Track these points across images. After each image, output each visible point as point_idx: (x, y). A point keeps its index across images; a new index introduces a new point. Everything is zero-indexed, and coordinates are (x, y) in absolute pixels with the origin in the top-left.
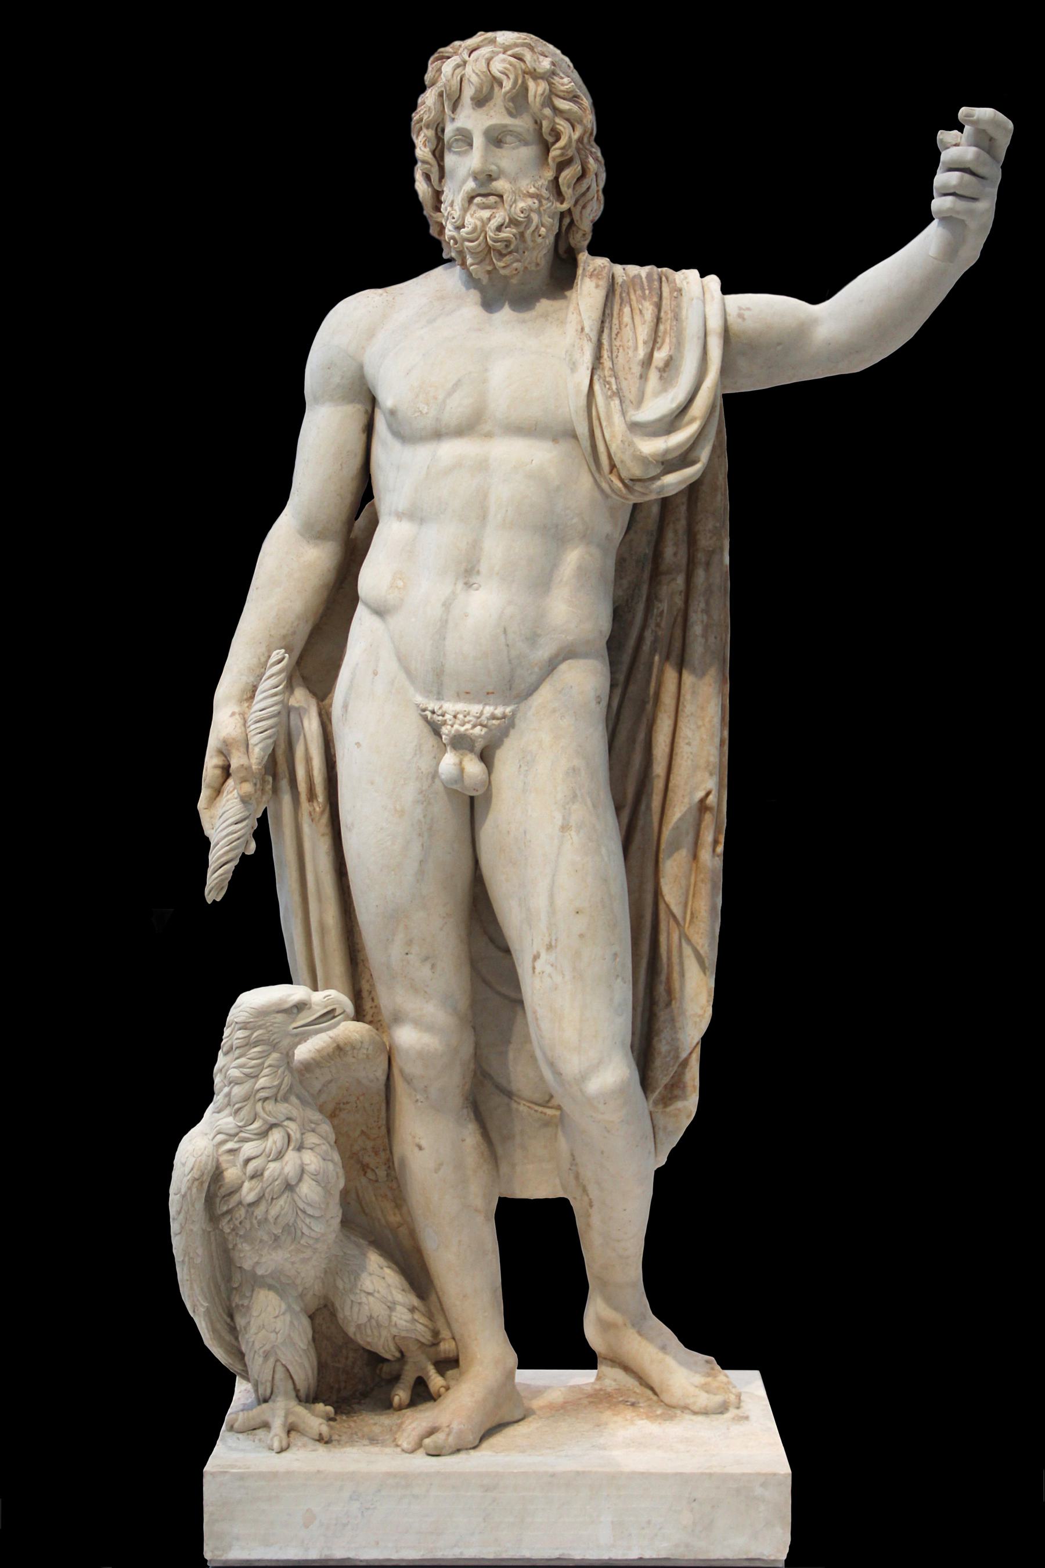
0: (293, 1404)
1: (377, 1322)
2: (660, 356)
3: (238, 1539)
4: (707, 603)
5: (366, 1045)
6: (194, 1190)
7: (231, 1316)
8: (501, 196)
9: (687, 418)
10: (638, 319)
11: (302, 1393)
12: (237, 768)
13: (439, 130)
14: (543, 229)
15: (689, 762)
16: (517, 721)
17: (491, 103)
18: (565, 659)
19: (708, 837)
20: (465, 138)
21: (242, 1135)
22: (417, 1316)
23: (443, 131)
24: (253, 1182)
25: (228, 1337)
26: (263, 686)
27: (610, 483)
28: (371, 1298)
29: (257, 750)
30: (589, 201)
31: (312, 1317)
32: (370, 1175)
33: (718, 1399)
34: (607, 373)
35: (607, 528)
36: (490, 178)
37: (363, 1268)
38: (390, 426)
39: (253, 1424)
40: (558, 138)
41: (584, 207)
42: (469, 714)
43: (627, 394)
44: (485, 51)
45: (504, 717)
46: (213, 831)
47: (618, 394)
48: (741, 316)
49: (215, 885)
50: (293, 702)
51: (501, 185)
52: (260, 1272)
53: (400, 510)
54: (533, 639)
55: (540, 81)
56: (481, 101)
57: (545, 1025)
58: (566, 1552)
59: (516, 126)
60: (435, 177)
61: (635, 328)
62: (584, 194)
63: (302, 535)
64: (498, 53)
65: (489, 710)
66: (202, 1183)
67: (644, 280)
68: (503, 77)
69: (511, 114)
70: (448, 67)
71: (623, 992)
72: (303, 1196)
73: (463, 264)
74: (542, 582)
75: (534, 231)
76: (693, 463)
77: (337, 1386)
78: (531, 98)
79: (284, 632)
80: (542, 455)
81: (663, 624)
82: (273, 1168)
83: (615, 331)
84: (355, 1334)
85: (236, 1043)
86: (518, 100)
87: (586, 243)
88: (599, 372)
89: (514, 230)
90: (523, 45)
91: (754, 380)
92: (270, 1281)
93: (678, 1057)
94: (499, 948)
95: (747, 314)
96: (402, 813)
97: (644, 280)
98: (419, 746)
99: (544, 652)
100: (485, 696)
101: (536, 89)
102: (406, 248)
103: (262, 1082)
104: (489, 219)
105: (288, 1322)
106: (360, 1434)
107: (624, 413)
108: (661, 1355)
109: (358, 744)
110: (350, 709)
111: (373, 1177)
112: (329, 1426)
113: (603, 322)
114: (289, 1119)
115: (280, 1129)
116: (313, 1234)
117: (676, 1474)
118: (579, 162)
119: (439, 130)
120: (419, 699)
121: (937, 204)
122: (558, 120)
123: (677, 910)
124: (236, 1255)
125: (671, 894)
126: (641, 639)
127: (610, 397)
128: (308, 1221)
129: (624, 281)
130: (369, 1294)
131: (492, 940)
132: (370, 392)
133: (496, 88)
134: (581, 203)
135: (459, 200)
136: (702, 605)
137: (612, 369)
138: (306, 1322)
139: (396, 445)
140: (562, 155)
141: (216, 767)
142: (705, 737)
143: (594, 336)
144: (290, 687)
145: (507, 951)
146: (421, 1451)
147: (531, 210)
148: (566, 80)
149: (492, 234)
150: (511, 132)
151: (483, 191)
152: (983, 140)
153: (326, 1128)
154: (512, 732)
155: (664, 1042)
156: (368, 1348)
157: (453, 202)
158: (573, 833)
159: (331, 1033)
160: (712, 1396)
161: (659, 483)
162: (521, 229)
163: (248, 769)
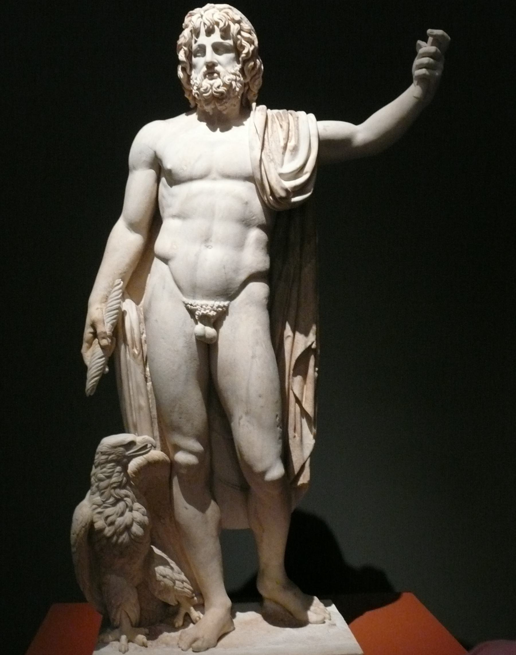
2: (291, 144)
11: (134, 623)
20: (202, 50)
23: (191, 47)
24: (110, 527)
31: (136, 587)
44: (212, 11)
45: (224, 306)
47: (272, 160)
48: (325, 129)
49: (91, 382)
70: (194, 18)
74: (240, 245)
79: (120, 272)
82: (119, 521)
86: (225, 33)
87: (256, 98)
99: (243, 277)
102: (173, 101)
103: (114, 479)
107: (276, 169)
121: (417, 72)
132: (159, 164)
141: (91, 333)
144: (123, 298)
146: (191, 649)
149: (215, 90)
152: (437, 41)
158: (257, 360)
159: (145, 456)
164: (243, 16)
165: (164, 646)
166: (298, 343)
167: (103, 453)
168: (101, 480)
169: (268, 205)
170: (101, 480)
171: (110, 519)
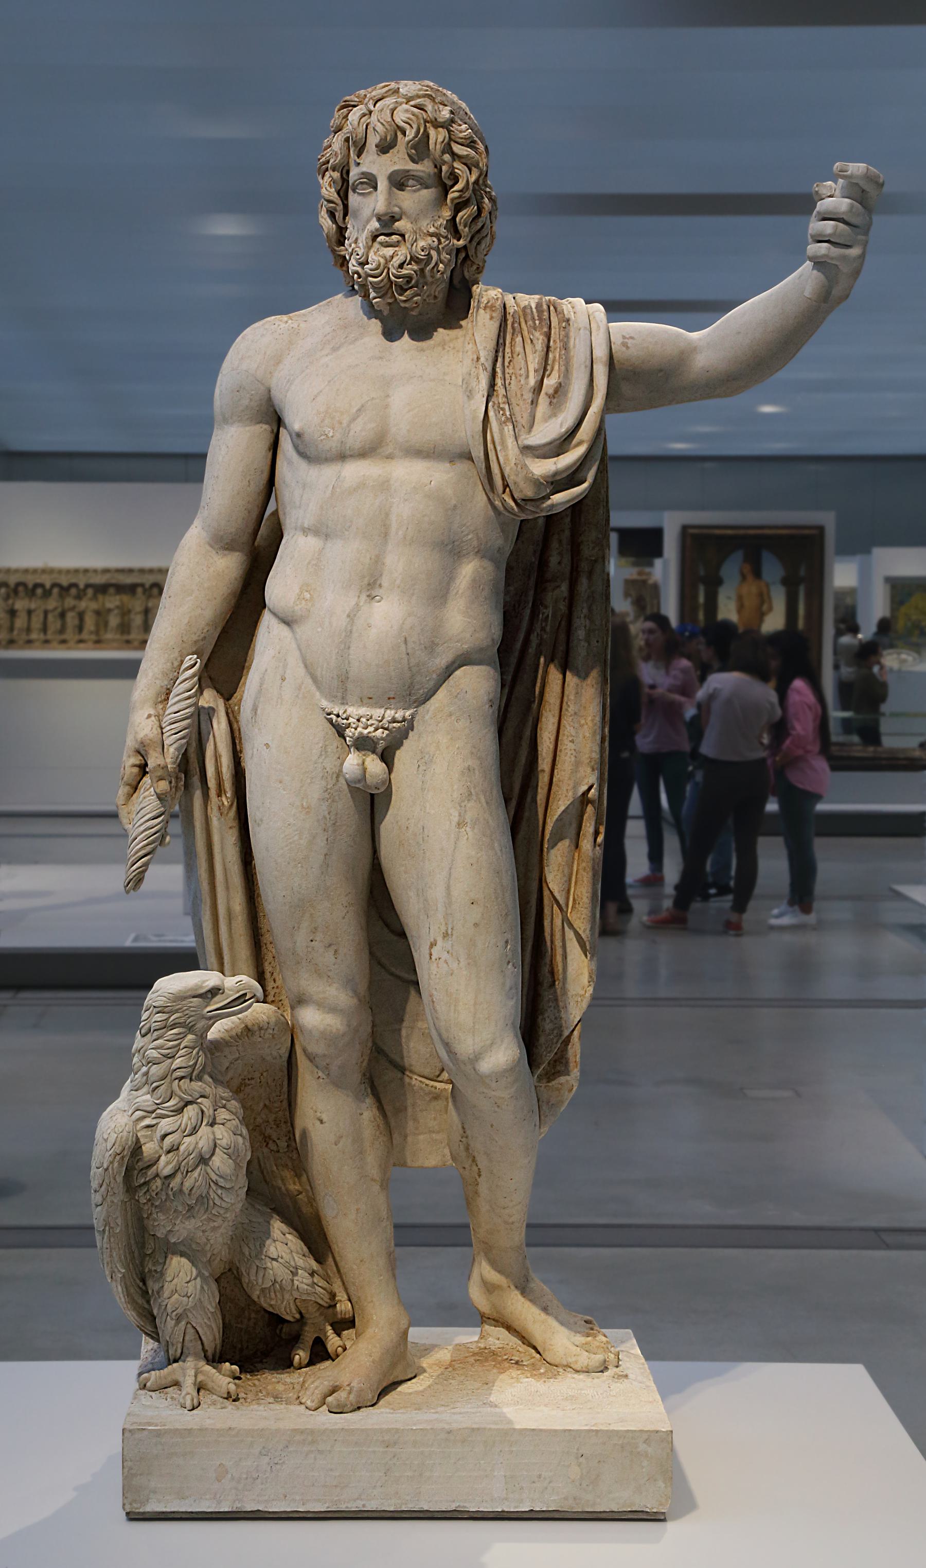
0: (202, 1363)
1: (281, 1287)
2: (550, 383)
3: (155, 1492)
4: (590, 610)
5: (272, 1024)
6: (116, 1164)
7: (144, 1281)
8: (403, 236)
11: (210, 1354)
12: (154, 768)
13: (344, 172)
14: (441, 265)
15: (573, 759)
17: (394, 150)
18: (460, 666)
19: (589, 827)
20: (371, 181)
22: (316, 1279)
23: (348, 172)
25: (140, 1301)
26: (178, 688)
27: (503, 501)
28: (274, 1263)
29: (172, 750)
30: (483, 238)
31: (217, 1280)
32: (272, 1146)
33: (599, 1357)
34: (501, 400)
35: (500, 542)
36: (394, 219)
37: (268, 1234)
38: (296, 447)
39: (164, 1382)
41: (479, 243)
42: (371, 718)
43: (519, 419)
44: (389, 101)
45: (404, 720)
46: (131, 826)
47: (512, 420)
48: (624, 344)
50: (202, 703)
53: (306, 525)
54: (431, 648)
55: (440, 129)
56: (385, 148)
57: (441, 1008)
58: (462, 1504)
59: (417, 171)
60: (339, 215)
62: (479, 231)
63: (211, 546)
64: (401, 104)
65: (389, 714)
66: (123, 1157)
67: (534, 310)
69: (414, 161)
71: (513, 975)
72: (215, 1169)
73: (366, 296)
74: (439, 595)
75: (433, 268)
77: (239, 1346)
78: (431, 146)
79: (195, 638)
81: (548, 629)
83: (507, 360)
84: (259, 1297)
86: (420, 149)
88: (494, 399)
89: (415, 267)
92: (182, 1248)
93: (561, 1035)
94: (393, 932)
95: (630, 342)
96: (307, 810)
97: (534, 310)
98: (325, 748)
99: (441, 661)
100: (388, 700)
103: (178, 1062)
105: (199, 1287)
106: (264, 1393)
108: (543, 1316)
109: (267, 745)
110: (259, 712)
111: (275, 1148)
112: (235, 1384)
113: (497, 351)
115: (195, 1105)
116: (224, 1205)
117: (565, 1431)
118: (475, 202)
119: (344, 172)
120: (325, 703)
122: (456, 165)
124: (149, 1223)
125: (554, 881)
126: (527, 641)
127: (505, 422)
128: (219, 1192)
129: (515, 311)
130: (273, 1259)
131: (387, 925)
134: (476, 240)
135: (364, 237)
136: (585, 611)
138: (214, 1286)
139: (302, 464)
140: (460, 197)
142: (588, 735)
143: (489, 366)
145: (402, 934)
147: (431, 248)
148: (464, 126)
149: (394, 271)
150: (414, 177)
155: (548, 1021)
156: (271, 1310)
157: (357, 239)
160: (593, 1356)
161: (549, 502)
162: (422, 266)
165: (271, 1400)
166: (558, 786)
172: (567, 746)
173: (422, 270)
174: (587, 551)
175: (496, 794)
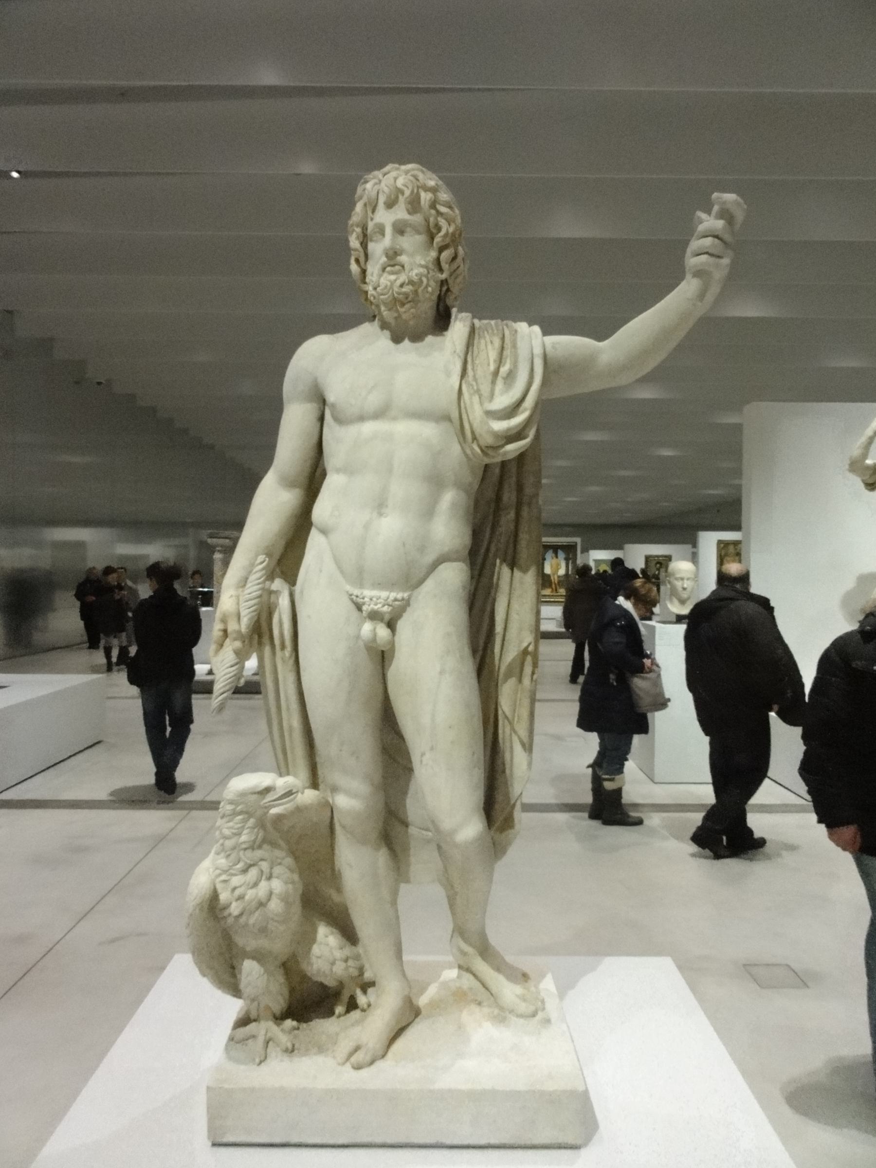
2: (504, 370)
8: (403, 267)
9: (521, 409)
10: (490, 347)
16: (411, 602)
21: (232, 871)
26: (253, 577)
27: (472, 449)
40: (439, 229)
41: (456, 278)
44: (394, 174)
45: (403, 599)
47: (478, 391)
48: (553, 347)
51: (403, 259)
52: (248, 949)
54: (422, 549)
56: (390, 205)
60: (362, 259)
61: (487, 351)
62: (455, 271)
65: (393, 595)
68: (405, 189)
69: (410, 213)
70: (369, 186)
71: (479, 775)
74: (429, 512)
76: (524, 438)
78: (422, 202)
80: (429, 431)
82: (250, 894)
85: (228, 812)
86: (414, 205)
90: (418, 170)
91: (561, 391)
99: (430, 558)
101: (425, 197)
103: (244, 838)
104: (396, 280)
107: (481, 404)
114: (262, 860)
120: (348, 588)
121: (692, 262)
122: (439, 219)
123: (508, 713)
126: (488, 550)
133: (400, 197)
137: (474, 376)
139: (337, 428)
141: (220, 630)
144: (271, 577)
150: (410, 225)
151: (392, 263)
152: (726, 215)
153: (289, 861)
154: (408, 609)
161: (503, 450)
163: (239, 632)
164: (440, 183)
167: (231, 802)
168: (226, 838)
169: (471, 456)
170: (226, 838)
171: (237, 892)
172: (514, 616)
173: (416, 292)
174: (528, 490)
175: (467, 651)
